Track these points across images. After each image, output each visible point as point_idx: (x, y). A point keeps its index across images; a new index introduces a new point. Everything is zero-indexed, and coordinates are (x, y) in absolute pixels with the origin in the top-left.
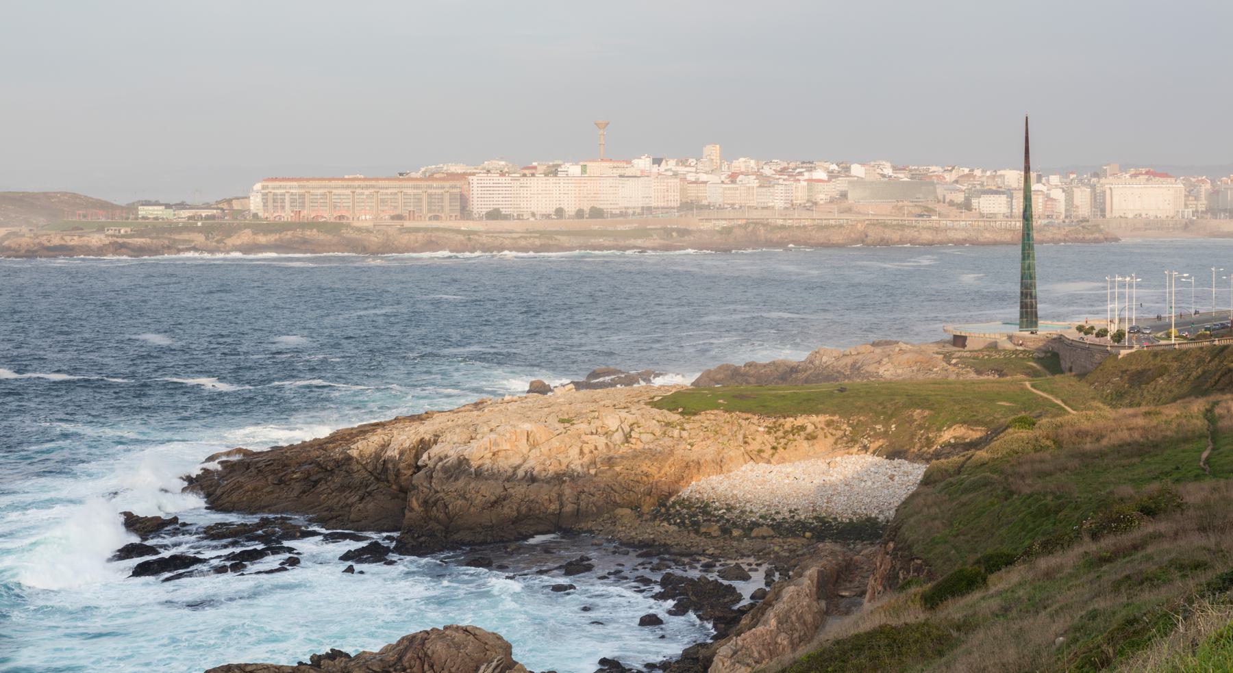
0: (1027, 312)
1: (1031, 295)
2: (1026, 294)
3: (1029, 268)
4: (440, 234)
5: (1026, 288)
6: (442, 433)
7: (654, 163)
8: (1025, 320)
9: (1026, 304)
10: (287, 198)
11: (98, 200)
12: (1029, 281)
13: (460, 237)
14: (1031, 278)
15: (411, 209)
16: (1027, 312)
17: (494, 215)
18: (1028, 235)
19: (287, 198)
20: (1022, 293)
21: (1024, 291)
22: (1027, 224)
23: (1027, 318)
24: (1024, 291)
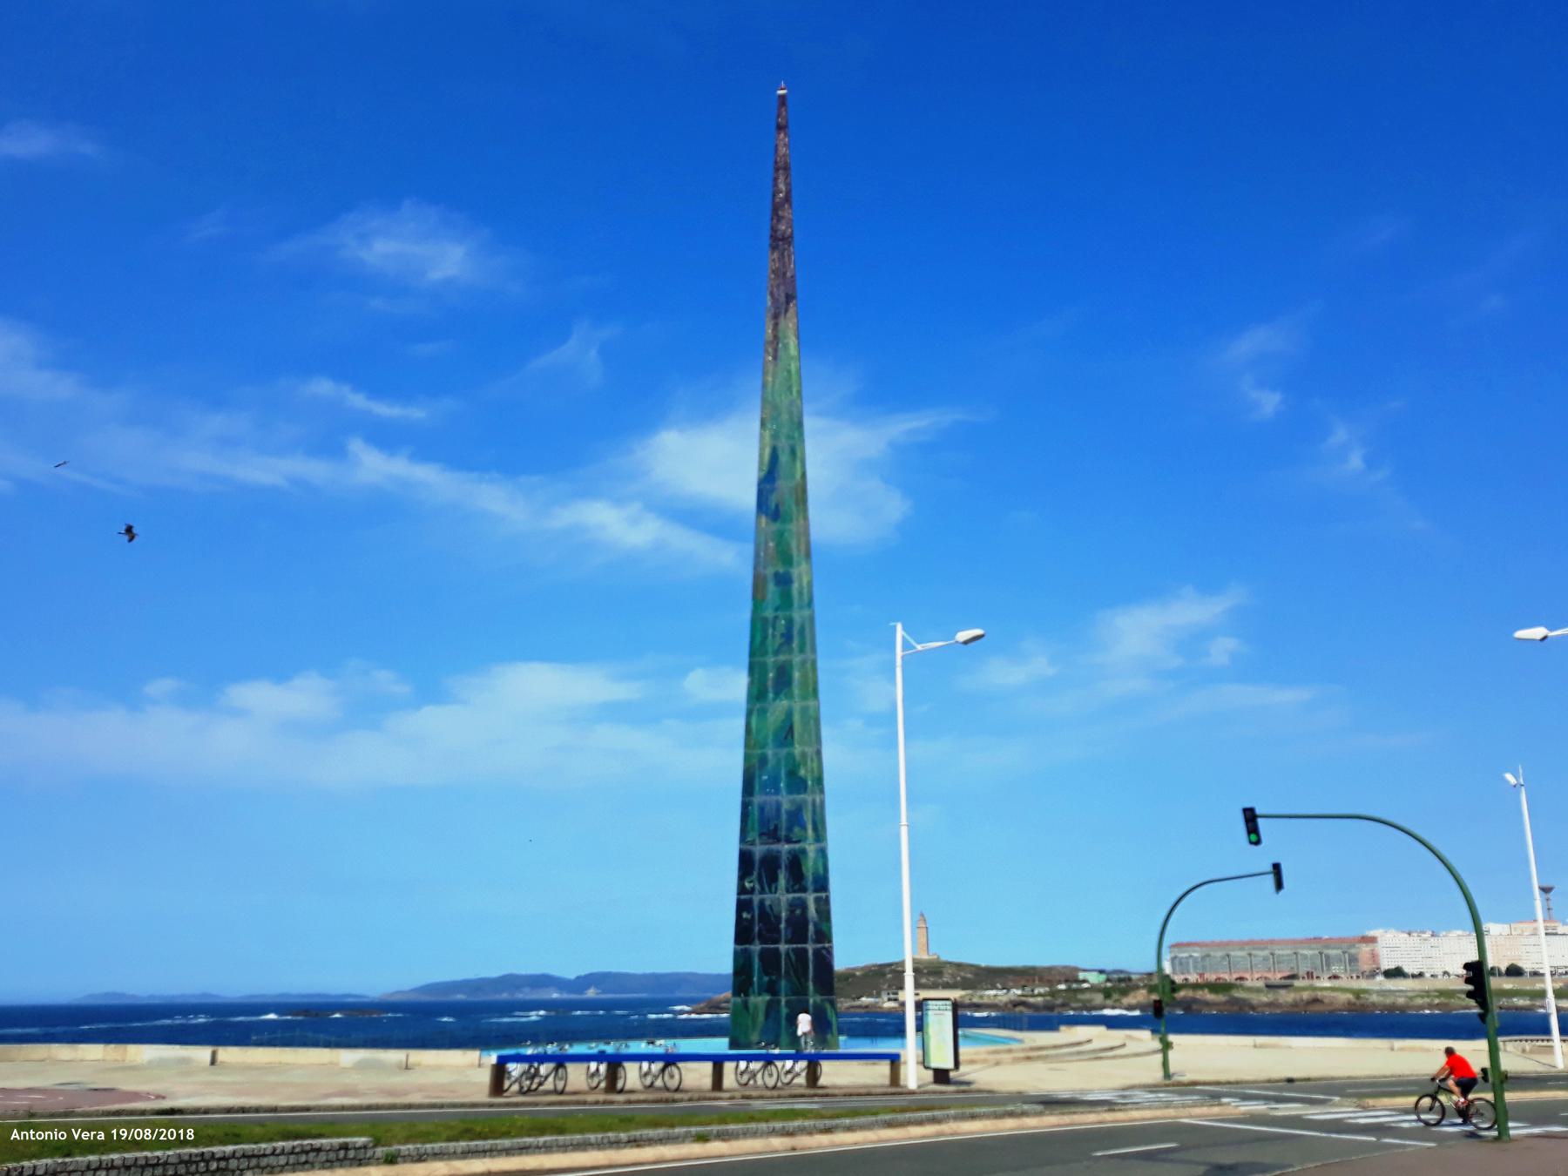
0: (770, 961)
1: (796, 863)
2: (770, 865)
3: (786, 734)
4: (1325, 993)
5: (772, 835)
6: (1548, 900)
7: (1467, 966)
8: (759, 1001)
9: (768, 918)
10: (1191, 961)
11: (666, 1144)
12: (786, 801)
13: (1350, 996)
14: (797, 784)
15: (1309, 970)
16: (770, 961)
17: (1396, 973)
18: (784, 581)
19: (1191, 961)
20: (745, 861)
21: (759, 850)
22: (780, 537)
23: (772, 989)
24: (759, 850)
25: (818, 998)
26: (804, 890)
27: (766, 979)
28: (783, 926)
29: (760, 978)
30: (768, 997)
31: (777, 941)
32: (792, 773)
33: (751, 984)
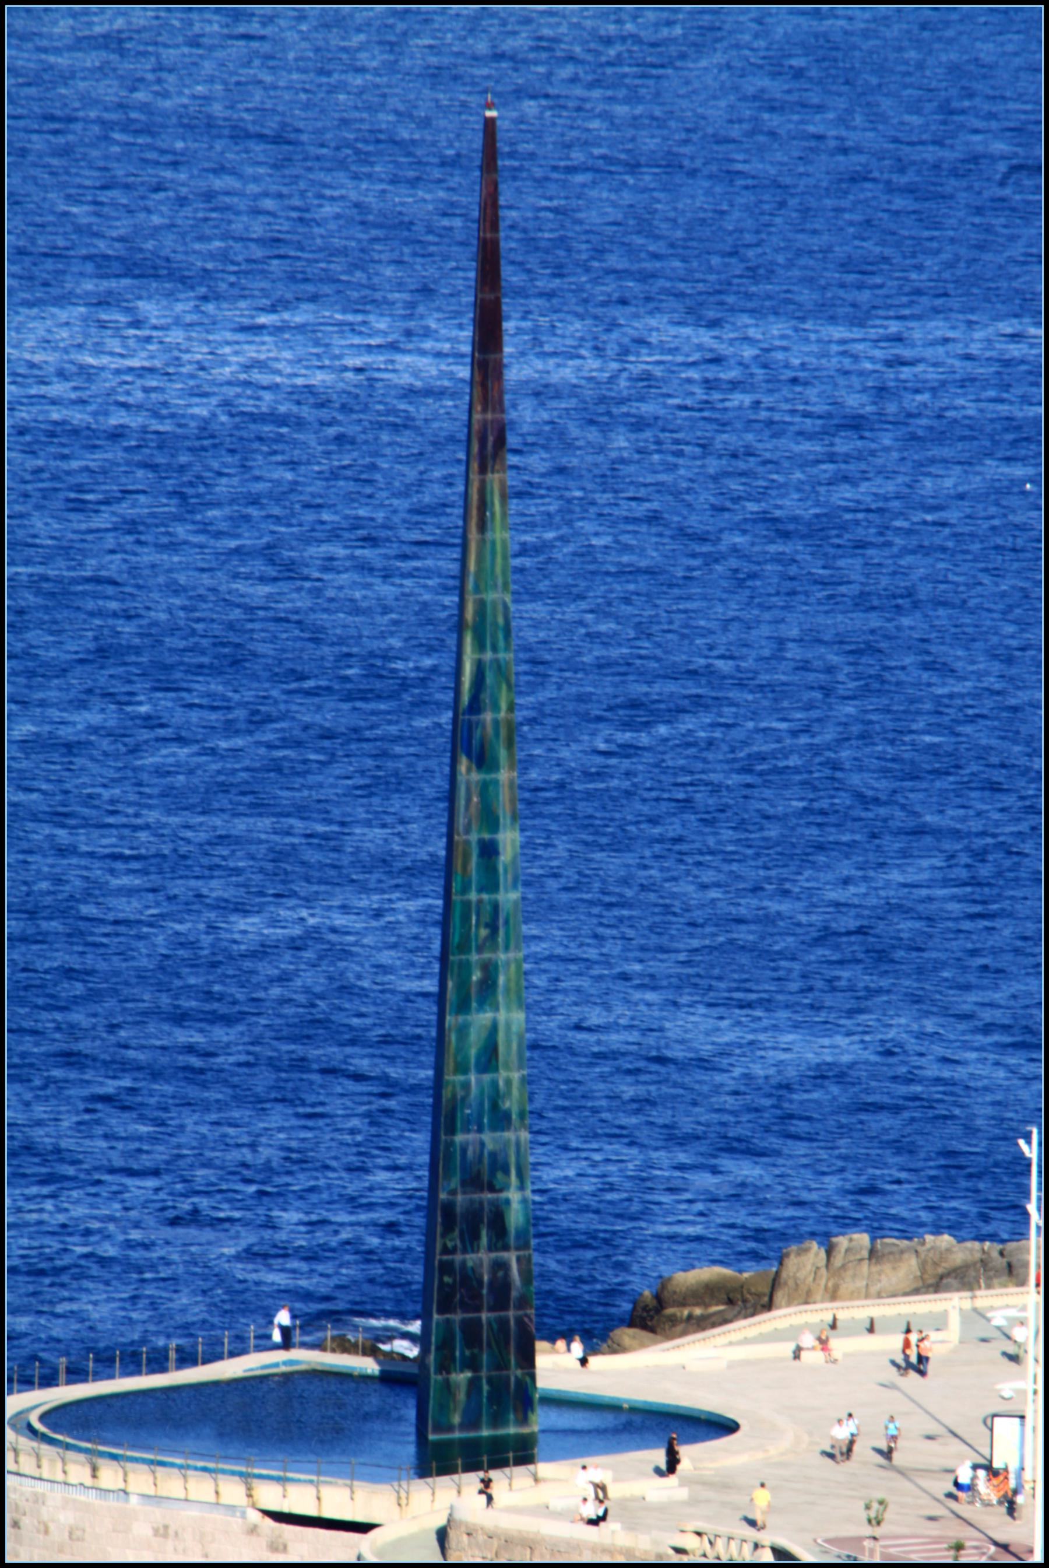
23: (472, 1364)
25: (519, 1372)
26: (506, 1248)
27: (467, 1353)
28: (485, 1291)
29: (462, 1354)
30: (469, 1374)
31: (478, 1309)
32: (495, 1106)
33: (453, 1358)
